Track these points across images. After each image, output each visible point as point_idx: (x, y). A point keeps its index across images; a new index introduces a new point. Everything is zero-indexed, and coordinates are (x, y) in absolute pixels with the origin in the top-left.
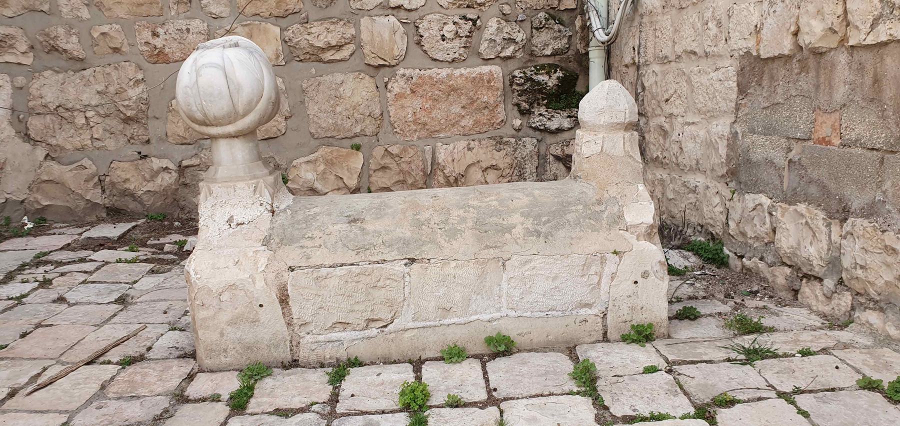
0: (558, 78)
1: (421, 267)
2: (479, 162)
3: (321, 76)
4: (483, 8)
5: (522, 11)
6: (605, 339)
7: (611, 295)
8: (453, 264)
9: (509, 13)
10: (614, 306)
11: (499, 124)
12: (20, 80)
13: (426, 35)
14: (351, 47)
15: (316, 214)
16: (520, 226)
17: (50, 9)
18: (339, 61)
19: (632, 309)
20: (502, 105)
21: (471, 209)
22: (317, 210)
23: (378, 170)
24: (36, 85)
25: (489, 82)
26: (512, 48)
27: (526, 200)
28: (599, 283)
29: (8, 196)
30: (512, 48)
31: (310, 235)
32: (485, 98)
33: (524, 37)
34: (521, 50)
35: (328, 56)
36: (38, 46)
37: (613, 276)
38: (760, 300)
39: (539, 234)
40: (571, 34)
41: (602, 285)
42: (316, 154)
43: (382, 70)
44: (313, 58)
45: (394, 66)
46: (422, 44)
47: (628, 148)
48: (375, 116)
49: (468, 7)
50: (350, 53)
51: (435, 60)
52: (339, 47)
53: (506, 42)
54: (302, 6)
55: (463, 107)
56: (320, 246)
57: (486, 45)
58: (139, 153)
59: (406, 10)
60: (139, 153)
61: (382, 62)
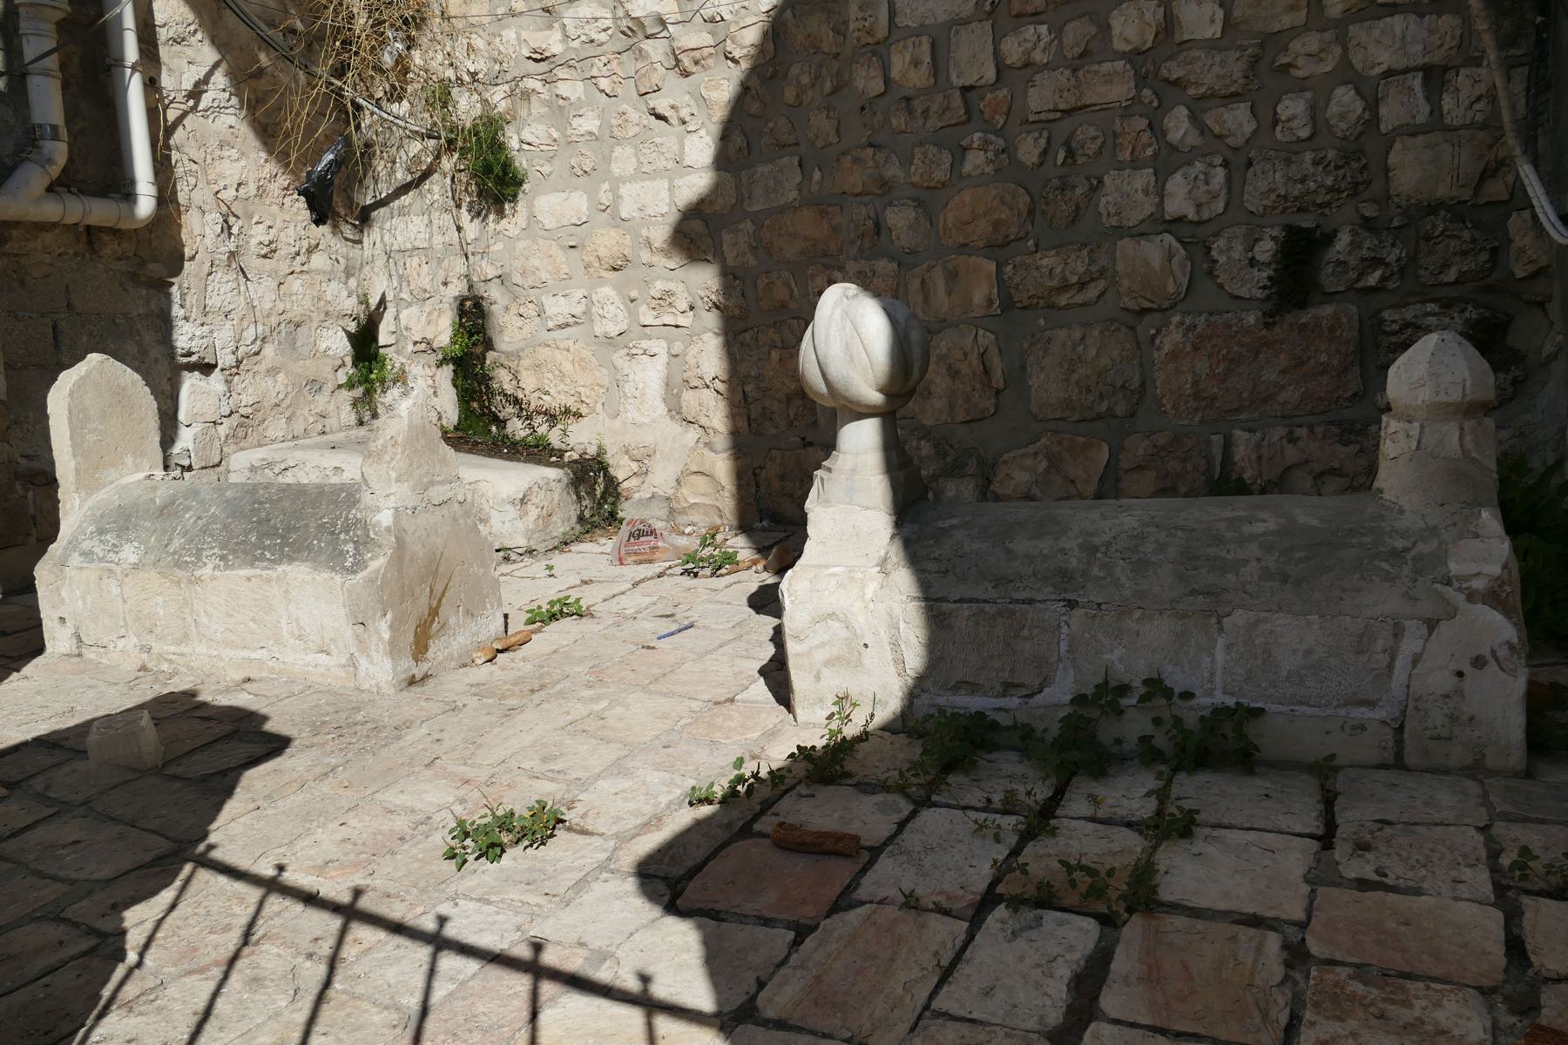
0: (1467, 321)
1: (1086, 614)
2: (1307, 462)
3: (1052, 329)
4: (1327, 211)
5: (1399, 211)
6: (1398, 763)
7: (1411, 690)
8: (1137, 614)
9: (1374, 215)
10: (1417, 709)
11: (1347, 400)
12: (678, 347)
13: (1222, 259)
14: (1101, 284)
15: (953, 527)
16: (1254, 564)
17: (1345, 83)
18: (1081, 305)
19: (1453, 719)
20: (1356, 369)
21: (1179, 533)
22: (954, 521)
23: (1133, 470)
24: (693, 350)
25: (1332, 329)
26: (1378, 274)
27: (1272, 524)
28: (1390, 666)
29: (655, 490)
30: (1378, 274)
31: (936, 555)
32: (1323, 358)
33: (1403, 255)
34: (1396, 276)
35: (1063, 300)
36: (699, 303)
37: (1416, 660)
38: (713, 575)
39: (1285, 579)
40: (1497, 244)
41: (1396, 672)
42: (1038, 444)
43: (1148, 318)
44: (1042, 302)
45: (1166, 309)
46: (1216, 273)
47: (1469, 444)
48: (1132, 387)
49: (1300, 210)
50: (1097, 293)
51: (1238, 298)
52: (1082, 285)
53: (1367, 263)
54: (1030, 227)
55: (1283, 372)
56: (947, 571)
57: (1330, 270)
58: (804, 439)
59: (1191, 222)
60: (804, 439)
61: (1147, 305)
